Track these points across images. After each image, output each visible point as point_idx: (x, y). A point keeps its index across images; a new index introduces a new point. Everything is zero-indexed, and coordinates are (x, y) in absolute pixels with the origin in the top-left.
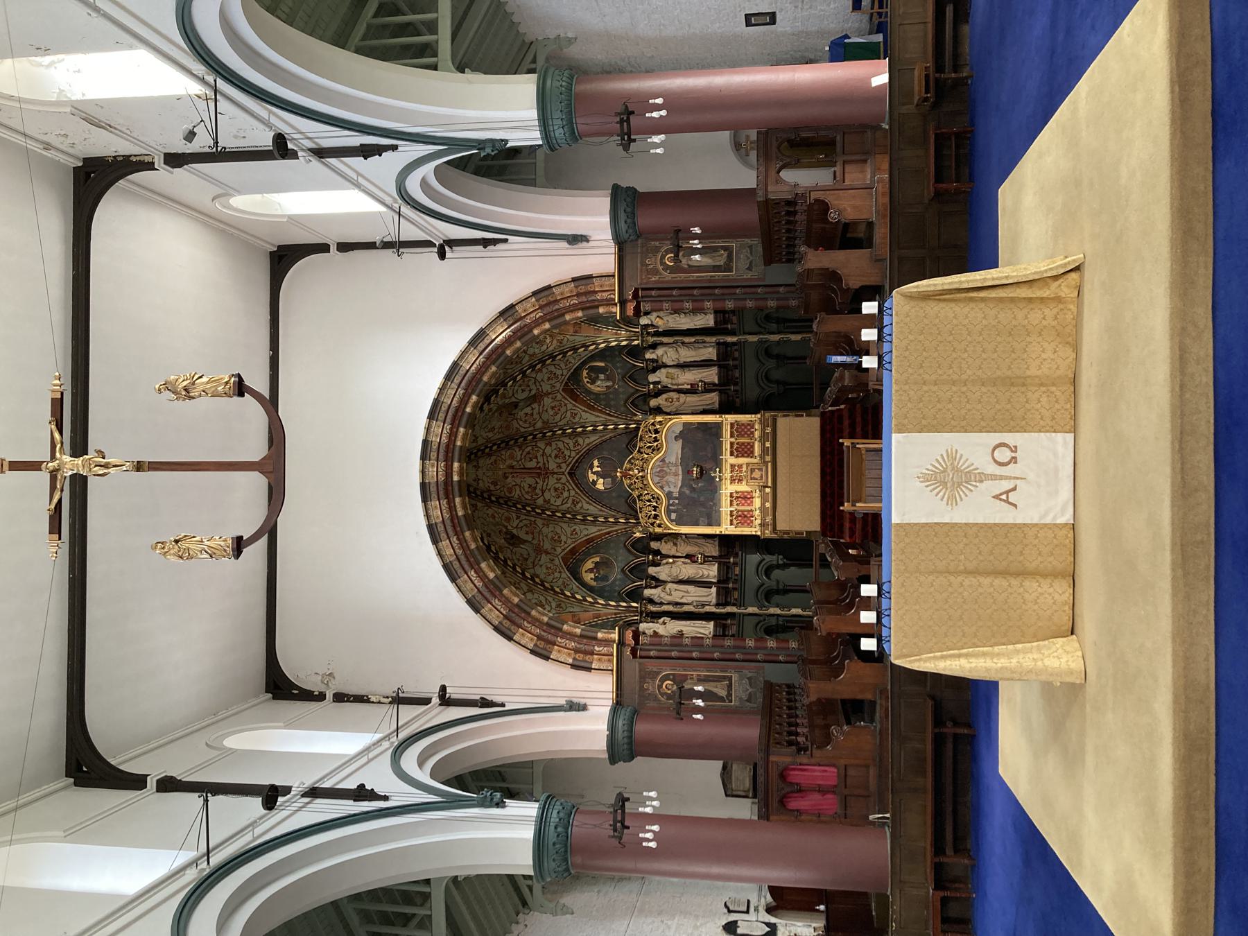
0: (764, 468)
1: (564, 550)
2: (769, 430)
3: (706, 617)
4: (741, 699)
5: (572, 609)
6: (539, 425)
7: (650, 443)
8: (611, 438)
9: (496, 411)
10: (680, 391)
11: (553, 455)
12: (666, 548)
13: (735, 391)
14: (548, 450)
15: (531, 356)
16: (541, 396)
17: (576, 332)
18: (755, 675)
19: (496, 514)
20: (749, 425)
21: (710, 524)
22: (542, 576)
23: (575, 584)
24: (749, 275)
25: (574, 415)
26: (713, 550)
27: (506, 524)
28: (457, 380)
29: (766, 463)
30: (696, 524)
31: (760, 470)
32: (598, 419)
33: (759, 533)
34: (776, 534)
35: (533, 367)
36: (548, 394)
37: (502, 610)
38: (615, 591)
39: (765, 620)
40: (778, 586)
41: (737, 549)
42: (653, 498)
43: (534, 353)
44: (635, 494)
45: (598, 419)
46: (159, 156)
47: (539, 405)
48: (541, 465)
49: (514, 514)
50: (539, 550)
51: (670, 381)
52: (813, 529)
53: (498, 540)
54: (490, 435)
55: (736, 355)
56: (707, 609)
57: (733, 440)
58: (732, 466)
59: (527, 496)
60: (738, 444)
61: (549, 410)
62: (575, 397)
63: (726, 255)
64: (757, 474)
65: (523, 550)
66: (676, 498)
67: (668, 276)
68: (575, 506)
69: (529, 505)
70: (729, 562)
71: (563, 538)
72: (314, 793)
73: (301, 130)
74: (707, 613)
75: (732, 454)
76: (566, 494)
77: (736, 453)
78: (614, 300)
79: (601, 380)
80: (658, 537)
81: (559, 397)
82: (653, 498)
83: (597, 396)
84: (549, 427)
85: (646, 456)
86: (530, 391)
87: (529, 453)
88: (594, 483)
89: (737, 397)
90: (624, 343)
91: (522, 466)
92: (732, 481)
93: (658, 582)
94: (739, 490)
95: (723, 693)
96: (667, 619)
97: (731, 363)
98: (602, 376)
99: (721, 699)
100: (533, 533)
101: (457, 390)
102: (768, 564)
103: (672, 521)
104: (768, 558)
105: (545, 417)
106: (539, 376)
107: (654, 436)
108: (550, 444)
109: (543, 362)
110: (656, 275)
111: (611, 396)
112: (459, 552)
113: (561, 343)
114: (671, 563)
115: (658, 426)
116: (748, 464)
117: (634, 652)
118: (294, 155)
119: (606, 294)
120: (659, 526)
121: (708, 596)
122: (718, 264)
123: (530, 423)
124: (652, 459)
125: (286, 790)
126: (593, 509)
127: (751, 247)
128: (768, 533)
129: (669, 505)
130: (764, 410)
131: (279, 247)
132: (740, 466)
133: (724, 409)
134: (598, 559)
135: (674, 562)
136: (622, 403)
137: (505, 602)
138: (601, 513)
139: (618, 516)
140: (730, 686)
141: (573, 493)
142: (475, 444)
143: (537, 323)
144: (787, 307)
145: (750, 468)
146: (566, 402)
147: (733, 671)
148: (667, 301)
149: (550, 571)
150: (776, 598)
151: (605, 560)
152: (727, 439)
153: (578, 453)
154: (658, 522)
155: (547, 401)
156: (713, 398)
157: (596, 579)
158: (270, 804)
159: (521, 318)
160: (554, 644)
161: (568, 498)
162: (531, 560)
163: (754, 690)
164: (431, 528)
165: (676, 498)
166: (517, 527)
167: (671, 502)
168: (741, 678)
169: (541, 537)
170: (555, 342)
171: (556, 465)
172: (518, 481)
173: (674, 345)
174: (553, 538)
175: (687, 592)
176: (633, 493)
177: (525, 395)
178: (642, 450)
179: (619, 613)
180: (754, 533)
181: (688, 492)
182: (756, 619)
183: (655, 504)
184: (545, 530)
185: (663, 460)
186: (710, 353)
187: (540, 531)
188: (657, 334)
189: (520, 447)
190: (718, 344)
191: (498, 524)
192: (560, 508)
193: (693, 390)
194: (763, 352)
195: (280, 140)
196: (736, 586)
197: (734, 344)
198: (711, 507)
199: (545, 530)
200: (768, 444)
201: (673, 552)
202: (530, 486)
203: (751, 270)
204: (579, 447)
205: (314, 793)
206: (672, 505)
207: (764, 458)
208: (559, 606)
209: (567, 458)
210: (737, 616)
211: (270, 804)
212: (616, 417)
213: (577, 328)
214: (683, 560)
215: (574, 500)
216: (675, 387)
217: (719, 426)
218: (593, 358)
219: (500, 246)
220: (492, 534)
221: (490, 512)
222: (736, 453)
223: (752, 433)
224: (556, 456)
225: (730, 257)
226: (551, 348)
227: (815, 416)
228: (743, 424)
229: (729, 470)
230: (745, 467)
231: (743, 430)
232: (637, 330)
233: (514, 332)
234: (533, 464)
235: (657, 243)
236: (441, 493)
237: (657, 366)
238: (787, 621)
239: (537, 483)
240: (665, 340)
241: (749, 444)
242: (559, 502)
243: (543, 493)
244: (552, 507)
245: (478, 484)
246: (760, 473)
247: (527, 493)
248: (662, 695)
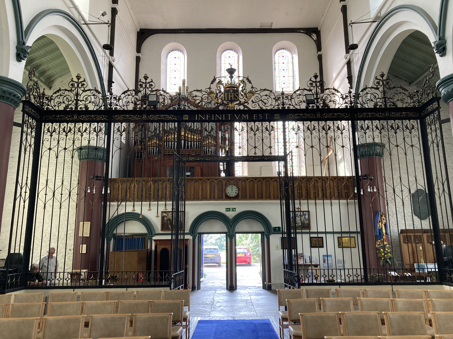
46: (346, 3)
72: (111, 67)
73: (358, 55)
118: (347, 52)
125: (112, 54)
131: (320, 31)
158: (106, 47)
195: (355, 47)
205: (111, 67)
211: (106, 47)
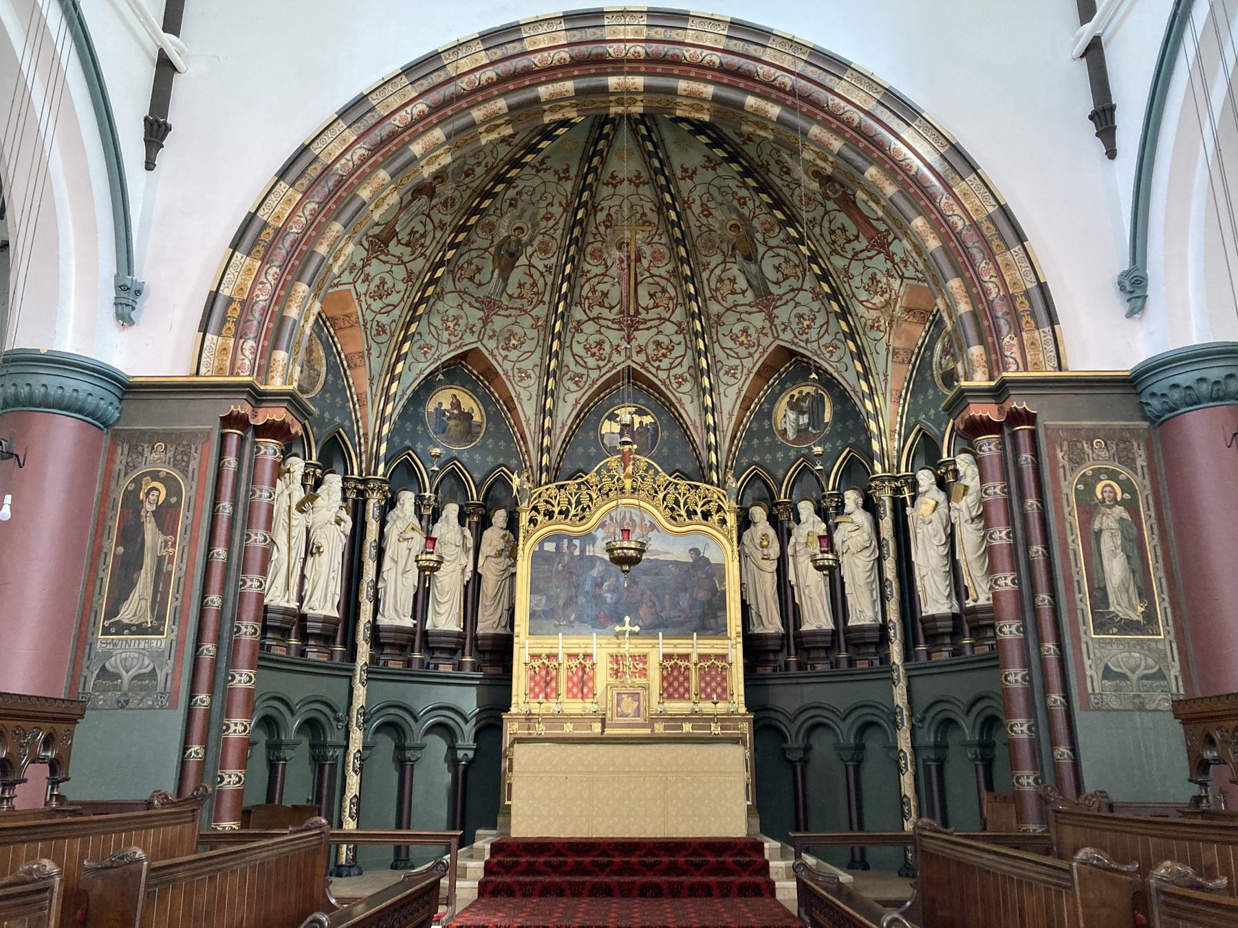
0: (640, 720)
1: (491, 353)
2: (716, 729)
3: (350, 604)
4: (109, 655)
5: (374, 353)
6: (714, 308)
7: (685, 503)
8: (692, 442)
9: (741, 216)
10: (782, 562)
11: (660, 338)
12: (494, 537)
13: (787, 664)
14: (669, 328)
15: (846, 270)
16: (767, 307)
17: (895, 353)
18: (160, 688)
19: (551, 223)
20: (724, 690)
21: (533, 615)
22: (440, 306)
23: (425, 366)
24: (1092, 671)
25: (733, 372)
26: (487, 624)
27: (536, 243)
28: (811, 72)
29: (651, 723)
30: (534, 590)
31: (637, 713)
32: (726, 416)
33: (513, 710)
34: (512, 745)
35: (824, 276)
36: (771, 318)
37: (343, 161)
38: (415, 443)
39: (337, 720)
40: (411, 748)
41: (489, 670)
42: (583, 510)
43: (851, 277)
44: (592, 477)
45: (726, 416)
47: (749, 305)
48: (643, 315)
49: (554, 260)
50: (489, 306)
51: (802, 540)
52: (513, 822)
53: (506, 221)
54: (697, 208)
55: (862, 665)
56: (366, 608)
57: (694, 658)
58: (643, 658)
59: (587, 288)
60: (687, 668)
61: (740, 326)
62: (765, 372)
63: (1135, 618)
64: (629, 706)
65: (489, 273)
66: (583, 551)
67: (1069, 486)
68: (571, 379)
69: (571, 288)
70: (463, 655)
71: (513, 355)
74: (358, 605)
75: (667, 657)
76: (591, 362)
77: (668, 664)
78: (1006, 370)
79: (797, 420)
80: (512, 524)
81: (765, 341)
82: (583, 510)
83: (766, 415)
84: (711, 327)
85: (661, 496)
86: (778, 283)
87: (664, 291)
88: (612, 417)
89: (775, 670)
90: (875, 446)
91: (640, 278)
92: (616, 658)
93: (429, 516)
94: (597, 670)
95: (126, 614)
96: (348, 525)
97: (843, 655)
98: (804, 419)
99: (113, 611)
100: (520, 297)
101: (792, 73)
102: (458, 731)
103: (541, 544)
104: (469, 729)
105: (730, 318)
106: (805, 297)
107: (699, 510)
108: (680, 331)
109: (835, 295)
110: (1070, 460)
111: (767, 439)
112: (464, 84)
113: (872, 327)
114: (464, 544)
115: (716, 517)
116: (646, 688)
117: (230, 421)
119: (1017, 356)
120: (533, 521)
121: (396, 611)
122: (1111, 598)
123: (717, 290)
124: (656, 507)
126: (566, 411)
127: (1160, 675)
128: (511, 728)
129: (570, 539)
130: (755, 721)
132: (643, 673)
133: (754, 647)
134: (477, 418)
135: (467, 551)
136: (756, 459)
137: (361, 173)
138: (559, 424)
139: (554, 454)
140: (140, 630)
141: (594, 374)
142: (679, 173)
143: (940, 224)
144: (1014, 765)
145: (639, 690)
146: (756, 356)
147: (173, 636)
148: (1007, 489)
149: (451, 324)
150: (387, 744)
151: (475, 430)
152: (696, 646)
153: (664, 383)
154: (540, 518)
155: (758, 319)
156: (771, 623)
157: (439, 412)
159: (948, 187)
160: (265, 260)
161: (586, 367)
162: (472, 288)
163: (125, 687)
164: (512, 30)
165: (583, 551)
166: (530, 265)
167: (577, 542)
168: (156, 655)
169: (514, 312)
170: (874, 314)
171: (643, 343)
172: (614, 271)
173: (875, 543)
174: (513, 334)
175: (405, 572)
176: (593, 473)
177: (771, 275)
178: (671, 488)
179: (366, 442)
180: (514, 700)
181: (595, 573)
182: (340, 701)
183: (573, 512)
184: (527, 321)
185: (653, 527)
186: (863, 612)
187: (526, 312)
188: (899, 508)
189: (675, 273)
190: (884, 628)
191: (535, 225)
192: (567, 352)
193: (784, 588)
194: (870, 718)
196: (415, 666)
197: (885, 659)
198: (567, 617)
199: (527, 321)
200: (687, 728)
201: (485, 549)
202: (605, 295)
203: (1104, 677)
204: (675, 386)
205: (165, 67)
206: (571, 545)
207: (657, 720)
208: (381, 329)
209: (656, 364)
210: (348, 665)
212: (730, 451)
213: (902, 356)
214: (470, 567)
215: (581, 376)
216: (790, 551)
217: (720, 631)
218: (842, 398)
219: (1099, 147)
220: (517, 212)
221: (557, 210)
222: (668, 664)
223: (709, 697)
224: (658, 344)
225: (1128, 626)
226: (860, 310)
227: (749, 825)
228: (724, 679)
229: (637, 651)
230: (643, 681)
231: (714, 679)
232: (903, 469)
233: (917, 180)
234: (644, 300)
235: (1141, 462)
236: (584, 50)
237: (829, 512)
238: (333, 766)
239: (611, 308)
240: (887, 524)
241: (687, 690)
242: (578, 349)
243: (593, 319)
244: (569, 335)
245: (607, 184)
246: (630, 711)
247: (593, 290)
248: (138, 481)
